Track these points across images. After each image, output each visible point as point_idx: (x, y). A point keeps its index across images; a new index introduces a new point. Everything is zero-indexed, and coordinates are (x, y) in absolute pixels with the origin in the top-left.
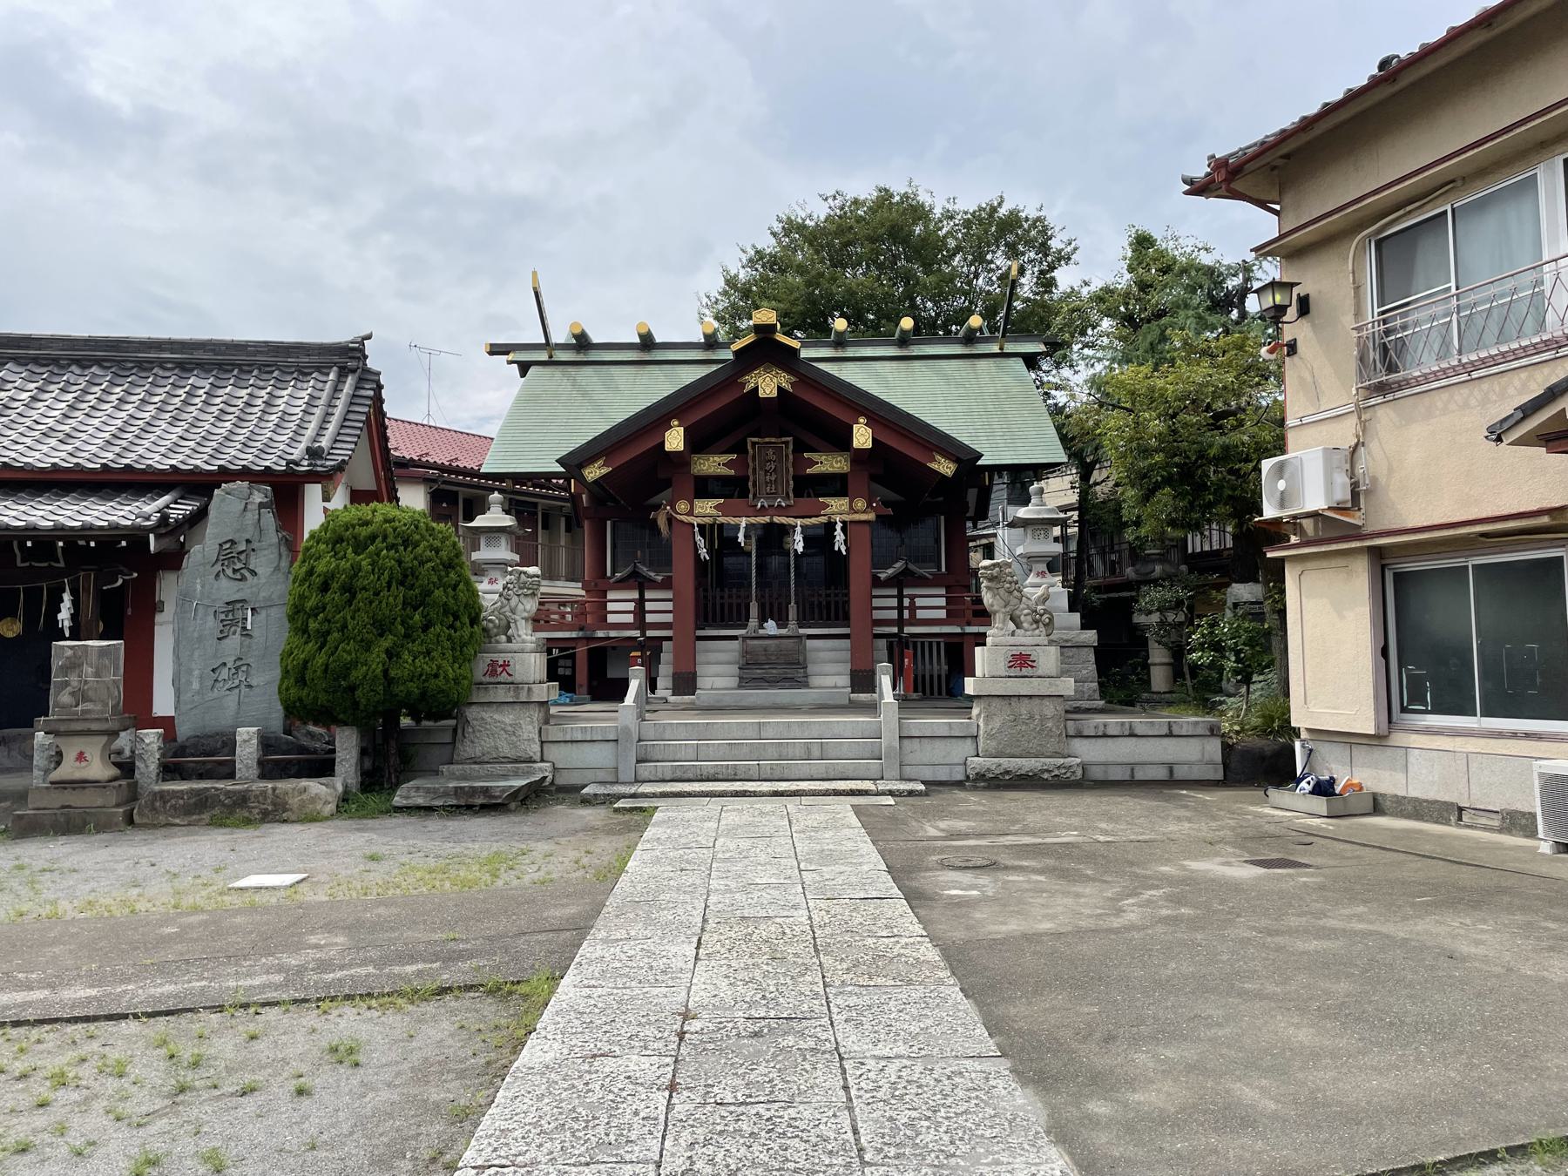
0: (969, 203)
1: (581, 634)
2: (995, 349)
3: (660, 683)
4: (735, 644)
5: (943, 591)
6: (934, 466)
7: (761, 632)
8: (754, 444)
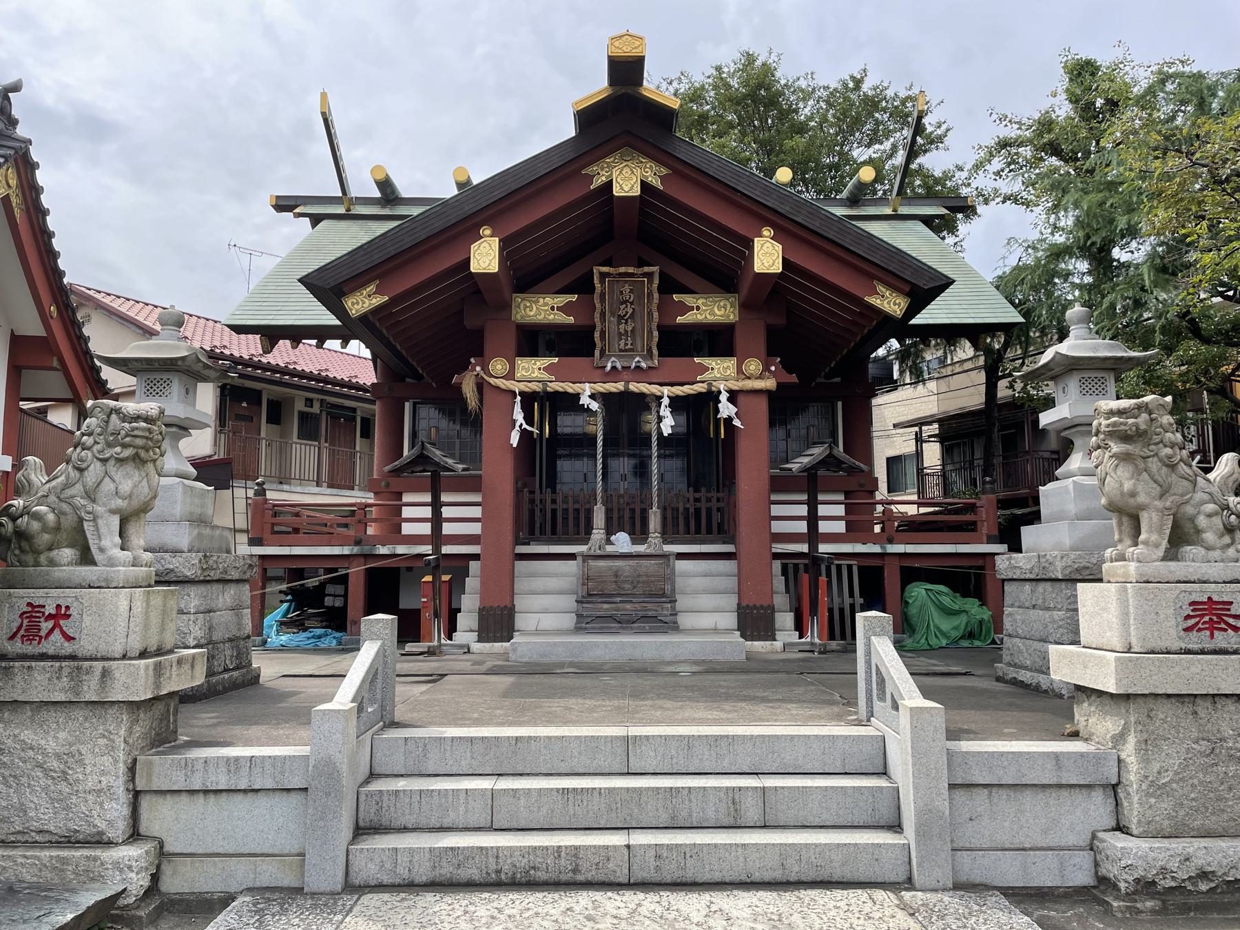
0: (830, 77)
1: (356, 550)
2: (888, 211)
3: (463, 620)
4: (571, 566)
5: (841, 497)
6: (875, 301)
7: (609, 549)
8: (603, 276)
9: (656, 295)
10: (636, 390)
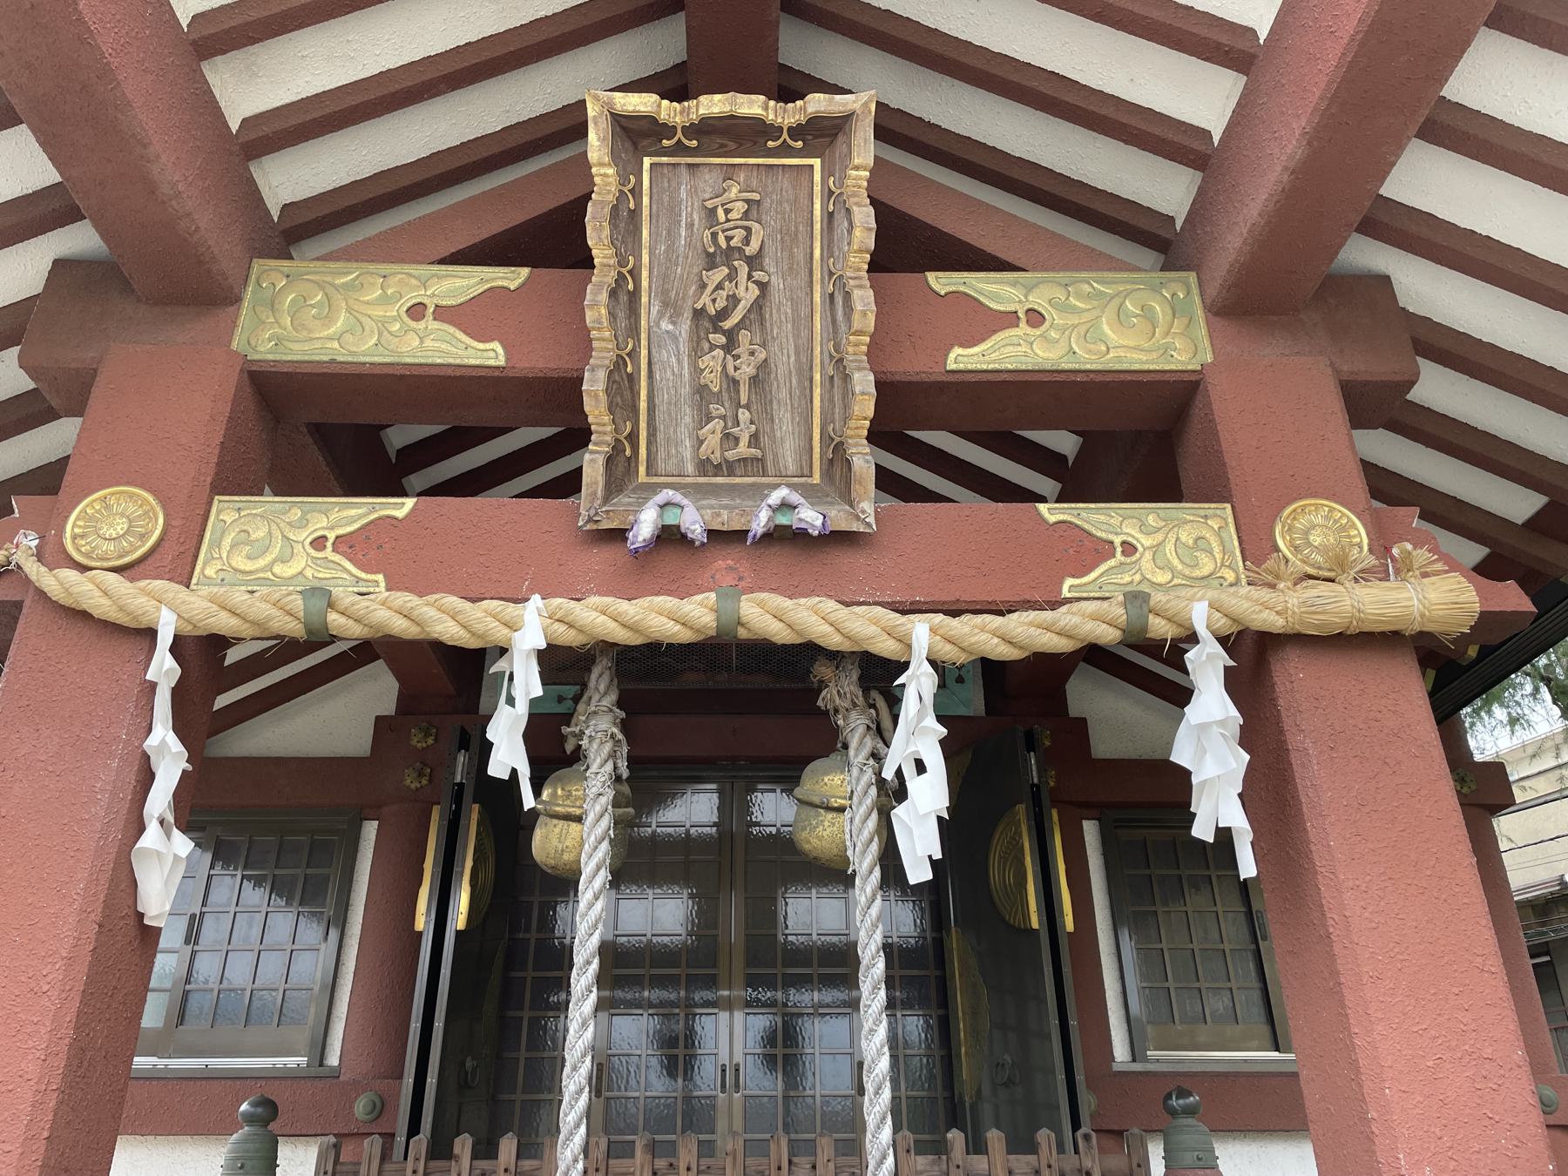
9: (864, 297)
10: (780, 634)
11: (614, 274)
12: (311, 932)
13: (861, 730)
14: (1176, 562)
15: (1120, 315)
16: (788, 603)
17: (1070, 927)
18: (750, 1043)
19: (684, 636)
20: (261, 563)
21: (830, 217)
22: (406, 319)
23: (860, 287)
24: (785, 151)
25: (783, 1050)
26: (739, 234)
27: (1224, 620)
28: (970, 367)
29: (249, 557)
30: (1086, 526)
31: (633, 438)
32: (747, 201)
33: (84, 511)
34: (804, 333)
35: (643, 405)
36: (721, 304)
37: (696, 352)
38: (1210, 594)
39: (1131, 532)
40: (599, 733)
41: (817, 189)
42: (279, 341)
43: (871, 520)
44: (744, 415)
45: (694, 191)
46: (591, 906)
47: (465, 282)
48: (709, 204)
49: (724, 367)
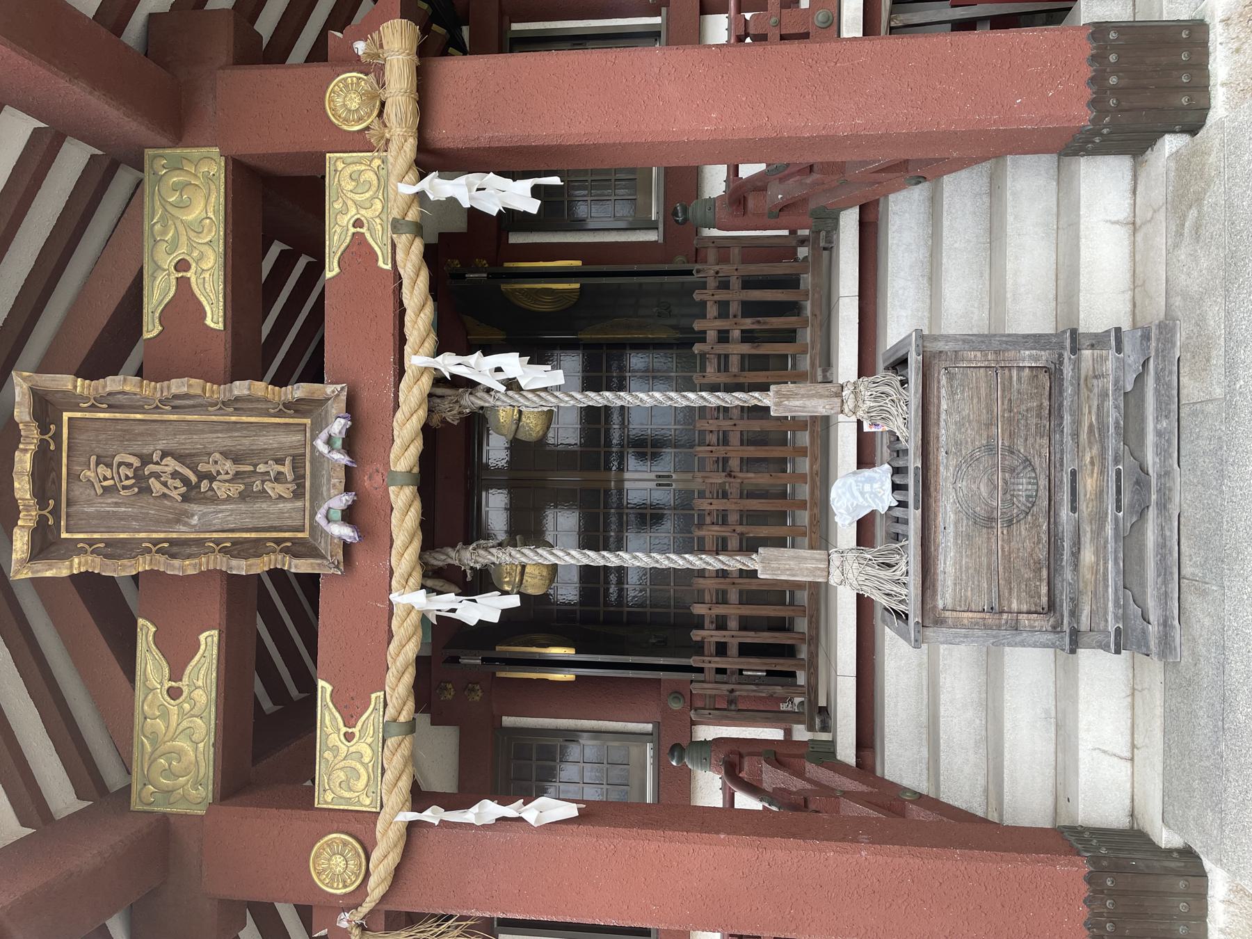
10: (416, 448)
11: (158, 556)
12: (574, 751)
13: (472, 398)
14: (367, 195)
15: (184, 206)
16: (398, 441)
17: (578, 263)
18: (644, 468)
19: (417, 506)
20: (362, 771)
21: (112, 407)
22: (181, 700)
23: (169, 388)
24: (57, 437)
25: (648, 447)
26: (123, 470)
27: (410, 175)
28: (221, 313)
29: (359, 778)
30: (342, 248)
31: (278, 541)
32: (97, 464)
33: (326, 885)
34: (201, 427)
35: (253, 535)
36: (178, 483)
37: (214, 500)
38: (393, 179)
39: (346, 220)
40: (470, 558)
41: (88, 415)
42: (197, 783)
43: (339, 387)
44: (261, 468)
45: (90, 503)
46: (573, 557)
47: (150, 663)
48: (100, 491)
49: (226, 481)
